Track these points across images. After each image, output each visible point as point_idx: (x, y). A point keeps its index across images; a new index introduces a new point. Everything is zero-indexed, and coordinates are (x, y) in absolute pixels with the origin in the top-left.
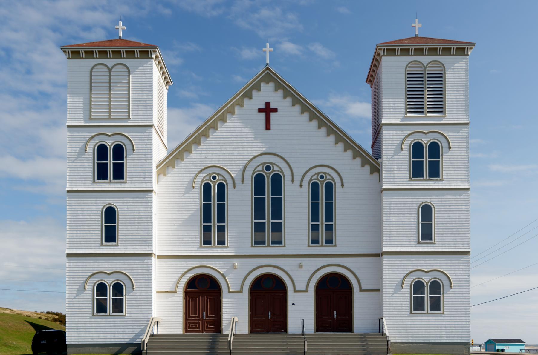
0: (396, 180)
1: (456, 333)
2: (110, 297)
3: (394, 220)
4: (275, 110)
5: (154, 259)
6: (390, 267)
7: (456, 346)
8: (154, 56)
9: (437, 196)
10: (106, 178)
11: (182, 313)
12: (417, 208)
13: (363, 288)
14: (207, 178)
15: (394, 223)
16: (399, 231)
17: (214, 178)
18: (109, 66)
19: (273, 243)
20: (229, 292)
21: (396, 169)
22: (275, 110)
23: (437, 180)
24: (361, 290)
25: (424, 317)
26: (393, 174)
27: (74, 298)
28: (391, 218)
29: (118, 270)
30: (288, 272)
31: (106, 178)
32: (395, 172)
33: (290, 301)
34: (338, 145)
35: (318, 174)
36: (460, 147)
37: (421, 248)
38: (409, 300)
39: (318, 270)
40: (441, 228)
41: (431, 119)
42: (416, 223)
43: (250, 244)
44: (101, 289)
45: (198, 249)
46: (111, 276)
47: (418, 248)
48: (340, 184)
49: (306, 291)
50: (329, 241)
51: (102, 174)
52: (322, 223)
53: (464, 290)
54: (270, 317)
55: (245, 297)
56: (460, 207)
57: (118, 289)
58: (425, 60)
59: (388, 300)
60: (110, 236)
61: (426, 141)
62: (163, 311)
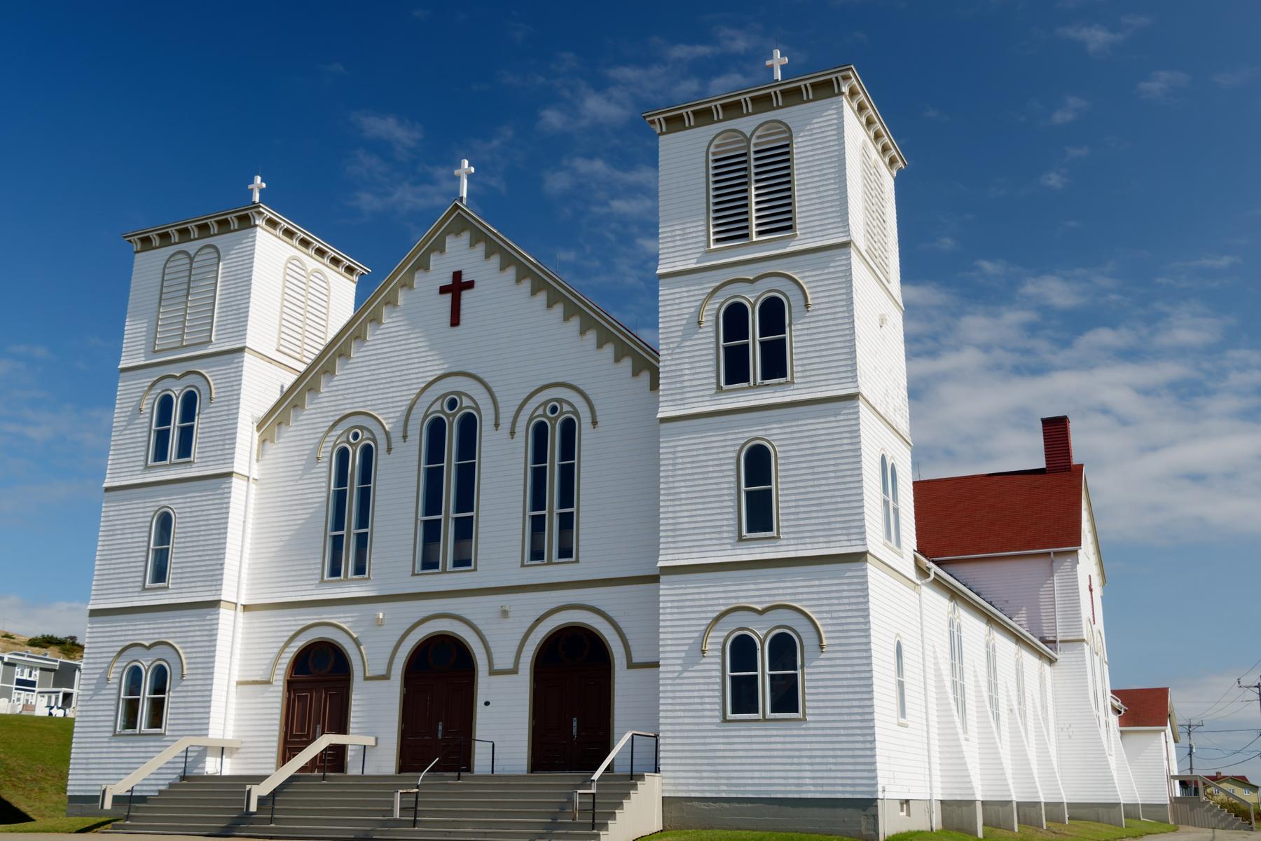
0: (687, 395)
1: (839, 774)
2: (148, 698)
3: (684, 490)
4: (470, 285)
5: (225, 614)
6: (676, 604)
7: (840, 812)
8: (845, 89)
9: (781, 422)
10: (746, 378)
11: (277, 728)
12: (734, 455)
13: (636, 659)
14: (343, 438)
15: (684, 496)
16: (696, 513)
17: (356, 436)
18: (744, 131)
19: (456, 564)
20: (366, 679)
21: (687, 372)
22: (470, 285)
23: (780, 384)
24: (631, 665)
25: (757, 731)
26: (682, 382)
27: (677, 678)
28: (676, 485)
29: (163, 638)
30: (480, 627)
31: (746, 378)
32: (686, 378)
33: (481, 696)
34: (585, 337)
35: (545, 403)
36: (831, 299)
37: (745, 551)
38: (718, 687)
39: (539, 620)
40: (793, 498)
41: (759, 246)
42: (734, 491)
43: (519, 559)
44: (742, 650)
45: (317, 587)
46: (152, 650)
47: (739, 552)
48: (589, 420)
49: (514, 671)
50: (463, 561)
51: (736, 370)
52: (449, 514)
53: (856, 654)
54: (440, 736)
55: (392, 692)
56: (837, 442)
57: (784, 649)
58: (746, 124)
59: (669, 688)
60: (759, 514)
61: (752, 298)
62: (234, 720)
